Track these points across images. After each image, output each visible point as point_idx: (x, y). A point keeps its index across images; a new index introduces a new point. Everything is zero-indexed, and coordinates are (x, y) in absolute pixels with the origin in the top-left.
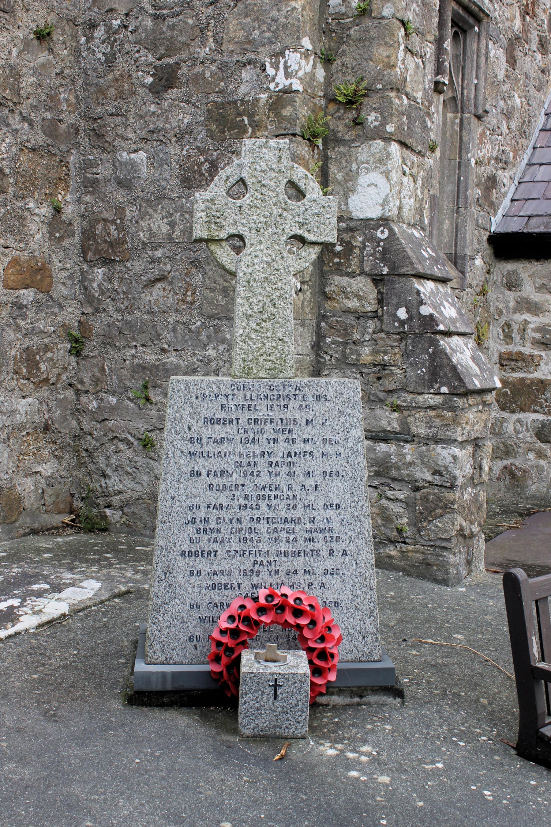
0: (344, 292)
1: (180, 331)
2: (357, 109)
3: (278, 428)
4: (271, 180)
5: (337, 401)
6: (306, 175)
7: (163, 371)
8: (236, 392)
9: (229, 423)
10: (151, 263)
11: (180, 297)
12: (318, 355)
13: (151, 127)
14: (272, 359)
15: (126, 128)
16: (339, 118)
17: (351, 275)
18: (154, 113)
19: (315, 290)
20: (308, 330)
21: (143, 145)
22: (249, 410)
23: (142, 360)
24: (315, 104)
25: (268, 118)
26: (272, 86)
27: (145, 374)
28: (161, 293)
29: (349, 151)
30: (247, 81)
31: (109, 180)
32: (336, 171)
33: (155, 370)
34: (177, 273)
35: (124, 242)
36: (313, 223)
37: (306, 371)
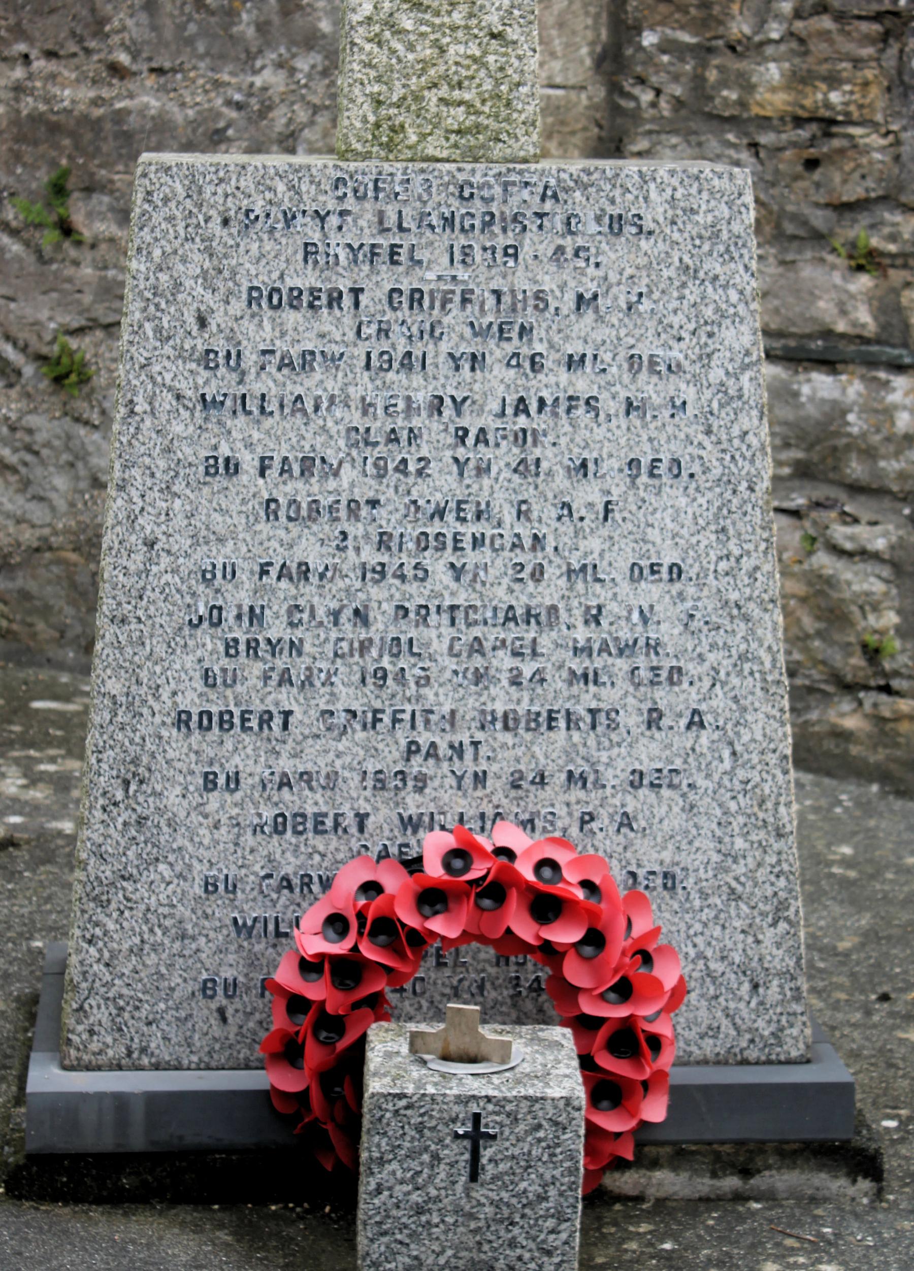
3: (485, 321)
5: (676, 236)
7: (116, 136)
8: (350, 203)
9: (330, 306)
12: (615, 88)
14: (467, 96)
22: (394, 262)
23: (47, 101)
27: (57, 146)
33: (89, 136)
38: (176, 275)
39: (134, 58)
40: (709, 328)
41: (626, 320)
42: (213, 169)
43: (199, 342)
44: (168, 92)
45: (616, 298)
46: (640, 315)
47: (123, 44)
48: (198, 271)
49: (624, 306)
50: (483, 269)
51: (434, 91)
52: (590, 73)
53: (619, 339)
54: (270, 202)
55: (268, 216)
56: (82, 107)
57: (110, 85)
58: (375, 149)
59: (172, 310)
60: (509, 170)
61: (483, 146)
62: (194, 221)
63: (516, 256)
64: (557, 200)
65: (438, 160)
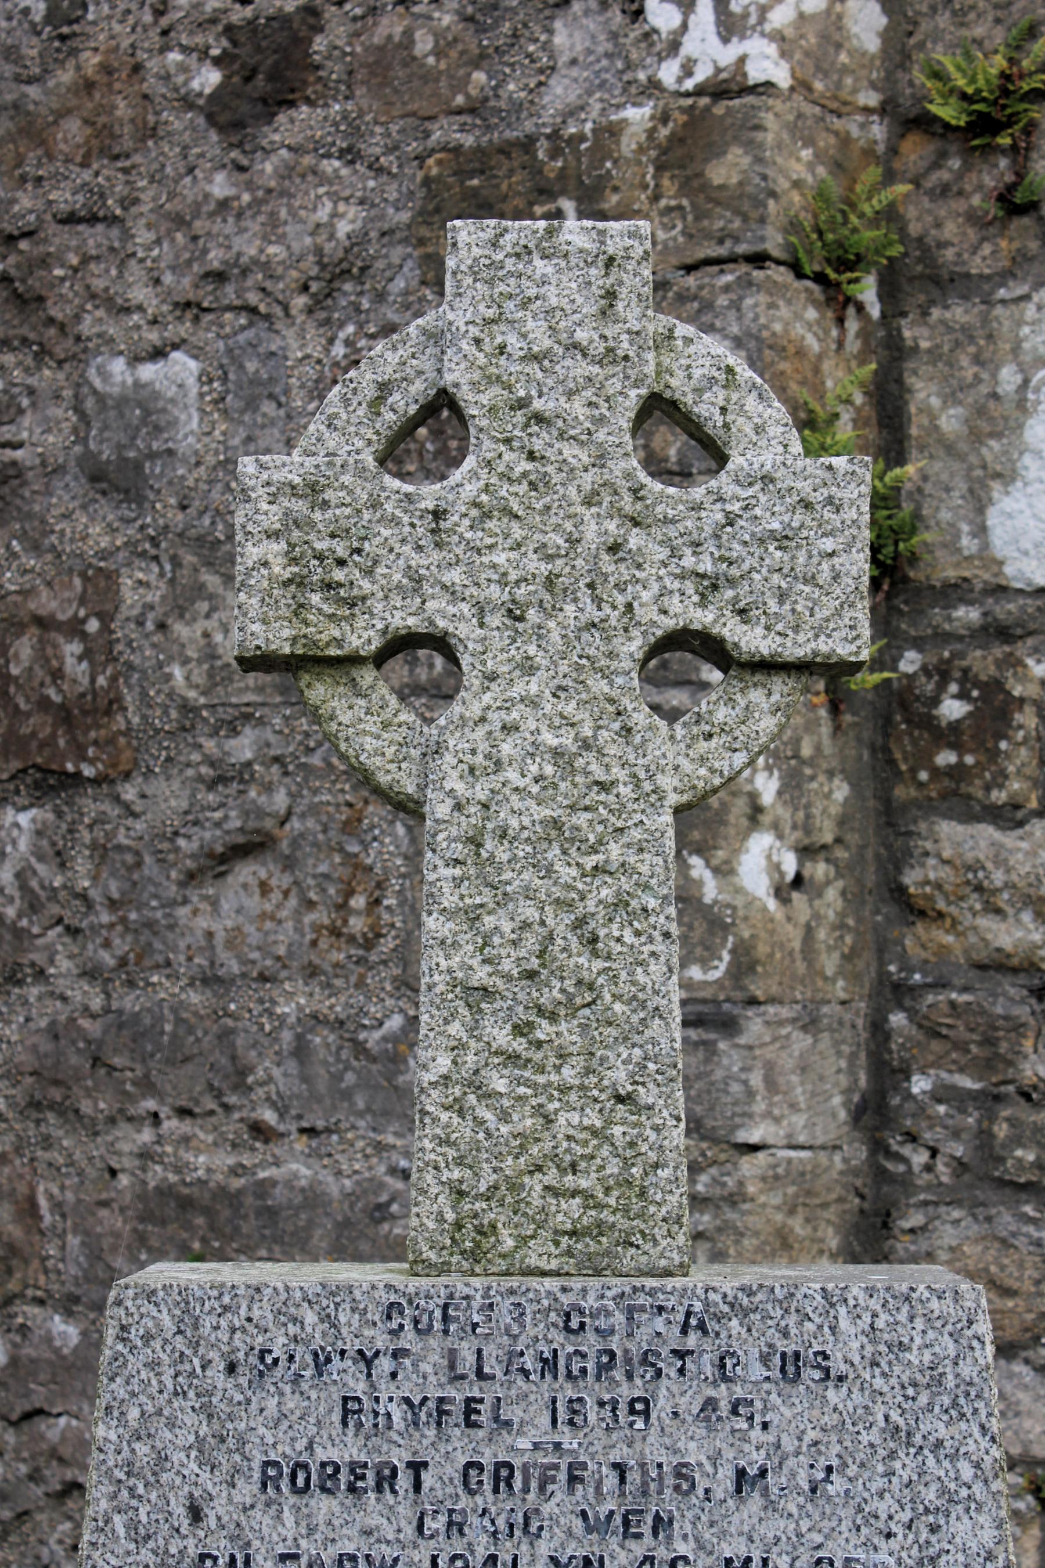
0: (979, 888)
1: (322, 1053)
2: (1014, 148)
3: (604, 1510)
4: (570, 394)
5: (879, 1383)
6: (730, 370)
7: (258, 1213)
8: (408, 1339)
9: (379, 1488)
10: (212, 785)
11: (321, 916)
12: (878, 1147)
13: (215, 258)
14: (584, 1183)
15: (122, 265)
16: (944, 191)
17: (1009, 816)
18: (224, 204)
19: (860, 882)
20: (836, 1044)
21: (185, 329)
22: (470, 1424)
23: (178, 1170)
24: (845, 140)
25: (656, 198)
26: (668, 73)
27: (188, 1226)
28: (254, 903)
29: (985, 319)
30: (574, 62)
31: (60, 470)
32: (935, 402)
33: (226, 1213)
34: (310, 823)
35: (114, 704)
36: (762, 573)
37: (831, 1214)
38: (159, 1445)
39: (281, 1116)
40: (931, 1519)
41: (809, 1507)
42: (215, 1293)
43: (191, 1542)
44: (320, 1157)
45: (793, 1475)
46: (829, 1498)
47: (268, 1099)
48: (192, 1438)
49: (806, 1487)
50: (599, 1432)
51: (538, 1176)
52: (846, 1129)
53: (799, 1535)
54: (295, 1340)
55: (291, 1358)
56: (219, 1177)
57: (253, 1149)
58: (455, 1259)
59: (153, 1496)
60: (635, 1289)
61: (607, 1253)
62: (187, 1367)
63: (646, 1414)
64: (705, 1332)
65: (544, 1274)
